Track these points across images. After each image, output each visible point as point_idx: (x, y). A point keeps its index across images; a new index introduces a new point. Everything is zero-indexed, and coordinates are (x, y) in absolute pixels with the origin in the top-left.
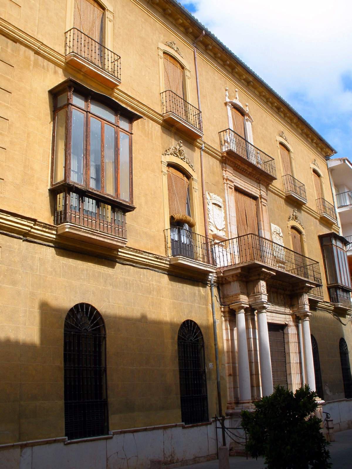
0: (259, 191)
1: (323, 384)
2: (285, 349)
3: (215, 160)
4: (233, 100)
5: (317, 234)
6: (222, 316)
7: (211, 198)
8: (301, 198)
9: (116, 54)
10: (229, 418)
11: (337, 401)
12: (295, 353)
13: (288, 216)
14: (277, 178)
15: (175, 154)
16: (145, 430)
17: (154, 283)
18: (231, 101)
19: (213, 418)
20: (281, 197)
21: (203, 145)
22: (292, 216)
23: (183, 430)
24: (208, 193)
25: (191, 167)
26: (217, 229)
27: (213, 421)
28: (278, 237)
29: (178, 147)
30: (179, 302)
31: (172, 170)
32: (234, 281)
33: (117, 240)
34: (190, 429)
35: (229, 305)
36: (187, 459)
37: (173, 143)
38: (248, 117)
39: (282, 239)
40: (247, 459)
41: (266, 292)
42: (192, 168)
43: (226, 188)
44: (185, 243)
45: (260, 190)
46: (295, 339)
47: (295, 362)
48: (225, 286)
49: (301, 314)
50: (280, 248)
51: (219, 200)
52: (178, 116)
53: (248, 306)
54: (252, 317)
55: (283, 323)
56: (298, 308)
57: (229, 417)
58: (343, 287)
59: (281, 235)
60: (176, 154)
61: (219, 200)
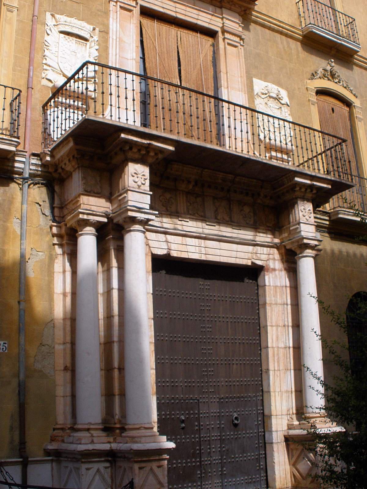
0: (220, 20)
2: (259, 318)
6: (54, 244)
7: (57, 22)
8: (340, 40)
10: (52, 461)
12: (284, 326)
13: (310, 69)
24: (53, 15)
28: (273, 104)
29: (329, 68)
37: (320, 64)
39: (285, 109)
41: (147, 187)
45: (222, 19)
46: (285, 297)
47: (282, 345)
49: (293, 243)
50: (276, 125)
51: (83, 27)
52: (318, 26)
53: (105, 220)
54: (119, 243)
56: (290, 232)
59: (285, 100)
61: (83, 27)
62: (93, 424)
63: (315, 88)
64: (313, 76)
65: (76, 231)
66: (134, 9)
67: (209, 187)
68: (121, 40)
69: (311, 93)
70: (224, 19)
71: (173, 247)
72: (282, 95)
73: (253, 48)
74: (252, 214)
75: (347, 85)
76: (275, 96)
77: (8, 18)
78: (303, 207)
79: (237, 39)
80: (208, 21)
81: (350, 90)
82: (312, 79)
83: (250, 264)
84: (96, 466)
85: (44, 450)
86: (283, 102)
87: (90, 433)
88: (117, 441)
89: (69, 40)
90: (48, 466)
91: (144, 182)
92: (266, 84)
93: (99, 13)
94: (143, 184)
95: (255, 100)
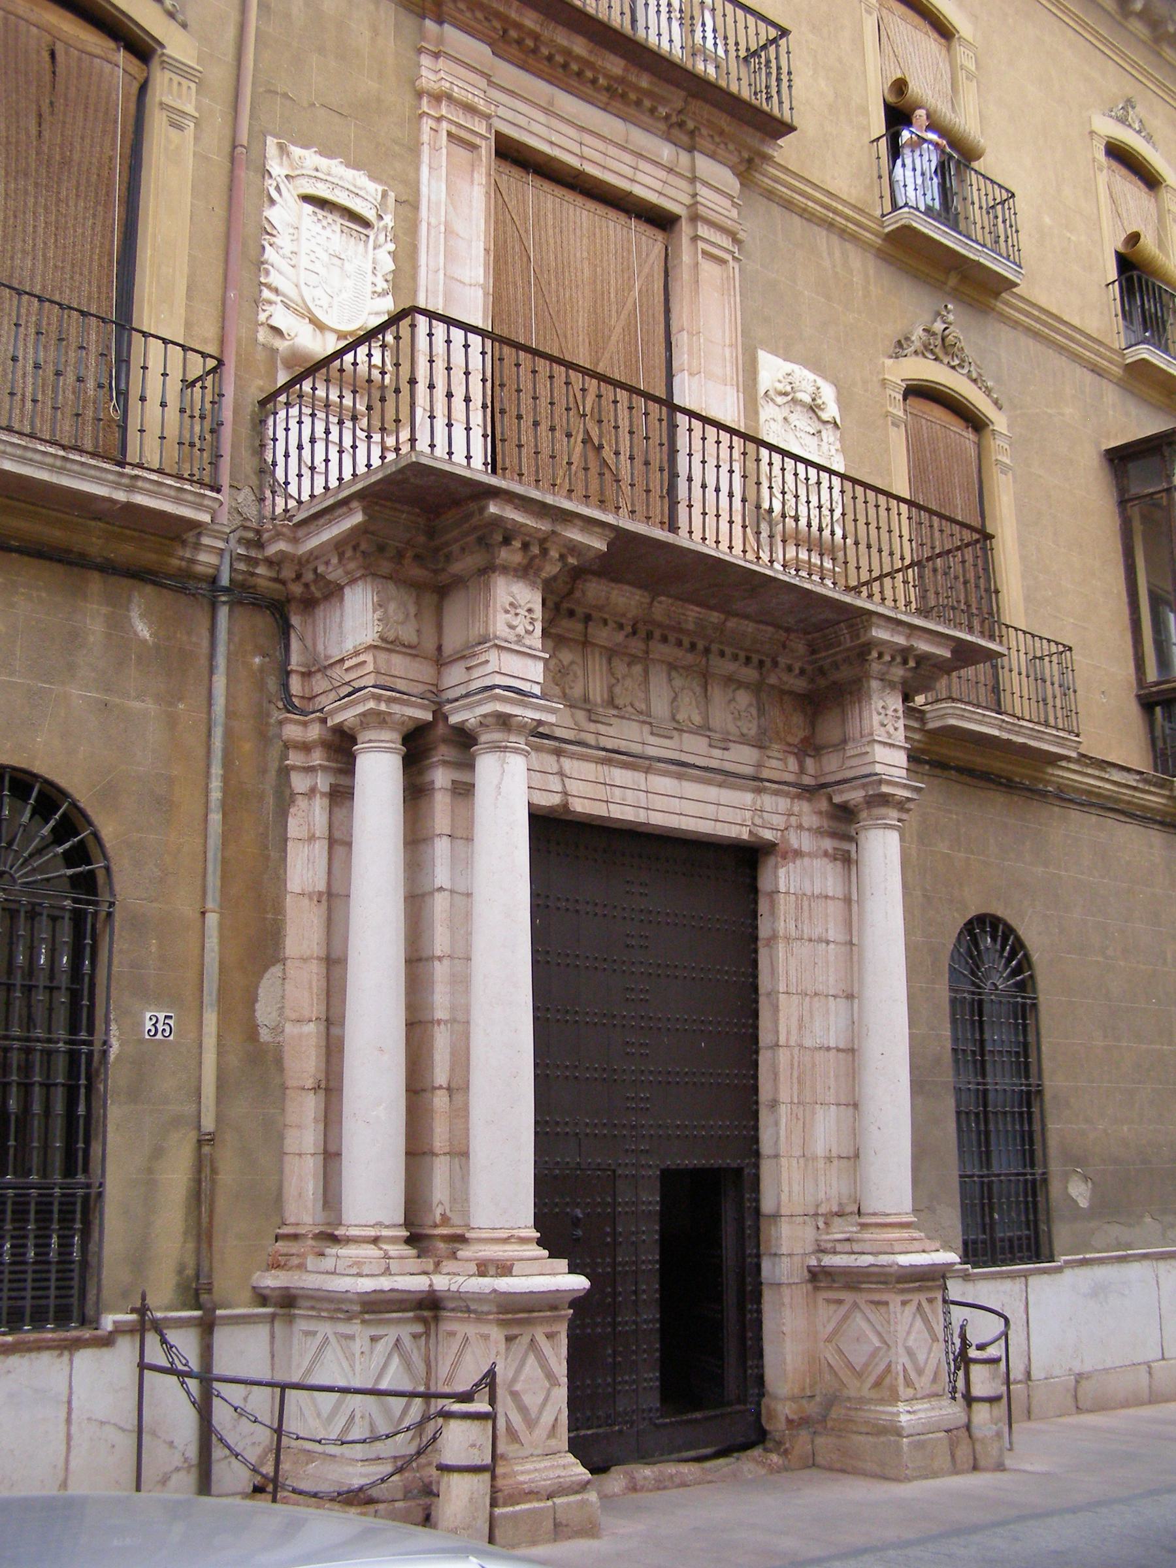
10: (273, 1317)
11: (1145, 1256)
13: (891, 330)
15: (926, 350)
19: (133, 1311)
20: (854, 238)
22: (918, 334)
24: (282, 148)
27: (119, 1330)
28: (801, 420)
31: (916, 403)
32: (353, 581)
33: (980, 718)
39: (829, 434)
41: (536, 640)
43: (425, 138)
48: (320, 612)
51: (360, 189)
59: (831, 411)
61: (360, 189)
62: (387, 1227)
64: (900, 347)
65: (354, 741)
66: (483, 143)
67: (664, 639)
68: (449, 231)
69: (894, 394)
70: (698, 185)
71: (573, 787)
72: (824, 399)
73: (762, 266)
74: (754, 711)
75: (980, 375)
76: (807, 399)
77: (172, 147)
78: (881, 704)
79: (726, 242)
80: (658, 185)
81: (987, 387)
82: (897, 358)
83: (745, 836)
84: (391, 1333)
85: (254, 1288)
86: (825, 416)
87: (381, 1249)
88: (445, 1271)
89: (325, 223)
90: (263, 1331)
91: (531, 628)
92: (789, 367)
93: (397, 148)
94: (527, 632)
95: (760, 410)
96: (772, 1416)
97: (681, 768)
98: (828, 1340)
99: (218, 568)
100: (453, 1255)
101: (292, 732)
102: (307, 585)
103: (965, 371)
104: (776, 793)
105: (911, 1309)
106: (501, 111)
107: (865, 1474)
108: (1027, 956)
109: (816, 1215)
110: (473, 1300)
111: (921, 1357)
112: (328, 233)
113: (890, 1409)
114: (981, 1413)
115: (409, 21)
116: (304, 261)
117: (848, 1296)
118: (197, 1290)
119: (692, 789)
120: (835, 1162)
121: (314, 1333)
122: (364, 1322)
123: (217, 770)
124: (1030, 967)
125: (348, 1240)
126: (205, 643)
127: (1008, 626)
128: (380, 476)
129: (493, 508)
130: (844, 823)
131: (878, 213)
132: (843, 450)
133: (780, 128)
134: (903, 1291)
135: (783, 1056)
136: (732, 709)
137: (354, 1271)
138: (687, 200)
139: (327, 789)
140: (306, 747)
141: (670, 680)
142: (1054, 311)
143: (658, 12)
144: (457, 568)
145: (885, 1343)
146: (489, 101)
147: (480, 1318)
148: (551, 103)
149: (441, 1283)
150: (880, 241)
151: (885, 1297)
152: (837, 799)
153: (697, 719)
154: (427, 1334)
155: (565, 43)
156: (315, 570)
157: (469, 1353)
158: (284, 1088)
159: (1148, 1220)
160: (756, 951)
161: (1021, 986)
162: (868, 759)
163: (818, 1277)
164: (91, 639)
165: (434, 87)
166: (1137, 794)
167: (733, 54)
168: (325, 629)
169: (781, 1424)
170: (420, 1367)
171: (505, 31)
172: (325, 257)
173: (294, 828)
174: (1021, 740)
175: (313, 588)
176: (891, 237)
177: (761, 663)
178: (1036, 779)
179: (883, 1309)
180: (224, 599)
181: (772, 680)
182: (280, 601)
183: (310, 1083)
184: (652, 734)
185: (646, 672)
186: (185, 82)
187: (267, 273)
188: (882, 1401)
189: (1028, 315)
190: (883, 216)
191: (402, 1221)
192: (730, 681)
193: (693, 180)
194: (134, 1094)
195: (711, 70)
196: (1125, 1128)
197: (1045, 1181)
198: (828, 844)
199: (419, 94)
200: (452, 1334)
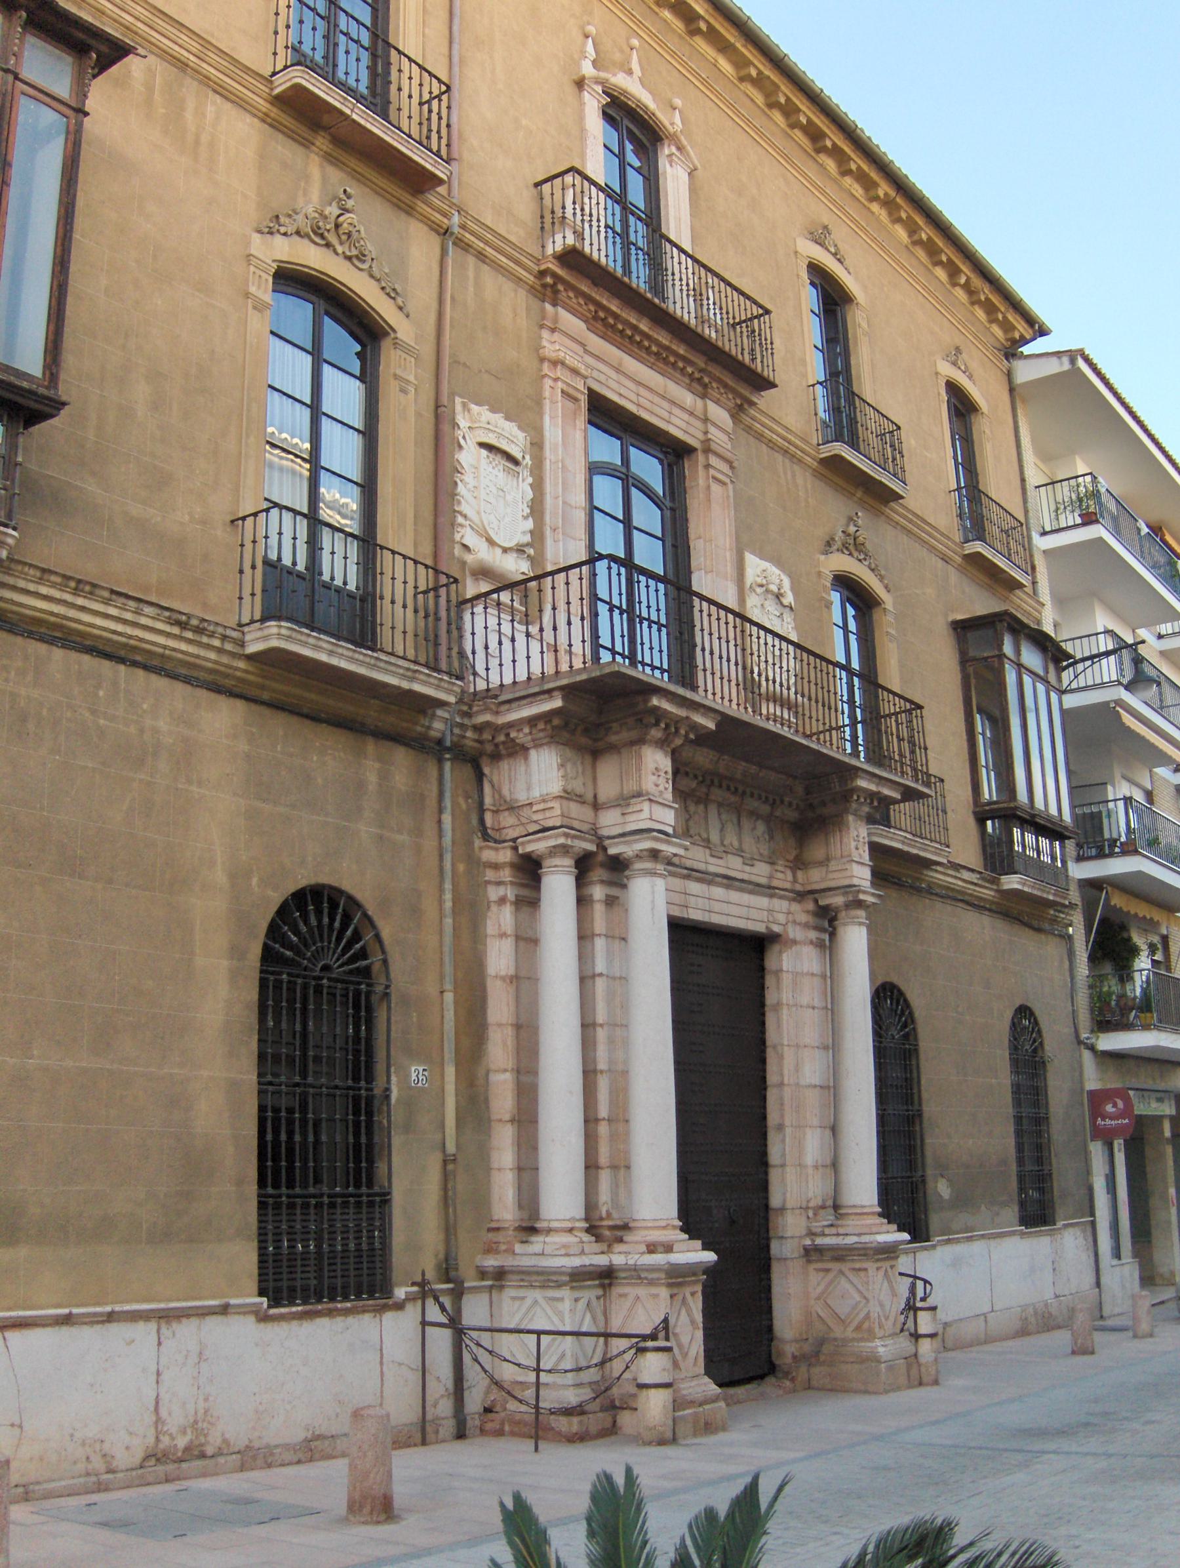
1: (929, 1172)
3: (508, 286)
4: (615, 75)
5: (946, 615)
9: (406, 56)
10: (491, 1287)
11: (983, 1236)
13: (821, 532)
14: (777, 382)
15: (317, 234)
16: (67, 1320)
17: (162, 725)
18: (603, 75)
19: (413, 1284)
21: (456, 219)
22: (839, 536)
23: (262, 1325)
24: (464, 405)
25: (392, 294)
26: (491, 542)
27: (410, 1298)
28: (771, 606)
30: (282, 809)
34: (295, 1323)
35: (514, 840)
36: (273, 1442)
38: (679, 149)
39: (788, 617)
40: (536, 1450)
41: (669, 795)
42: (394, 299)
43: (547, 394)
44: (338, 582)
51: (514, 439)
55: (760, 928)
57: (490, 1283)
58: (1034, 816)
59: (789, 599)
60: (322, 236)
61: (514, 439)
63: (274, 261)
76: (774, 588)
86: (785, 602)
96: (781, 1354)
97: (729, 881)
98: (818, 1298)
99: (444, 734)
100: (620, 1240)
101: (488, 855)
102: (497, 745)
103: (866, 563)
104: (781, 897)
105: (881, 1273)
106: (595, 374)
107: (856, 1392)
108: (911, 1014)
109: (808, 1208)
110: (643, 1270)
111: (887, 1308)
112: (495, 472)
113: (870, 1344)
114: (925, 1346)
115: (535, 303)
116: (483, 495)
117: (835, 1266)
118: (447, 1269)
119: (734, 896)
120: (821, 1169)
121: (523, 1298)
122: (572, 1288)
123: (448, 886)
124: (913, 1021)
125: (549, 1231)
126: (435, 789)
127: (382, 548)
128: (584, 677)
129: (655, 701)
130: (827, 920)
131: (815, 442)
132: (796, 628)
133: (763, 383)
134: (878, 1260)
135: (787, 1092)
136: (753, 837)
137: (563, 1252)
138: (701, 436)
139: (513, 899)
140: (496, 866)
141: (719, 814)
142: (919, 513)
143: (599, 232)
144: (613, 738)
145: (865, 1298)
146: (588, 366)
147: (652, 1283)
148: (620, 364)
149: (618, 1260)
150: (532, 278)
151: (864, 1265)
152: (821, 903)
153: (736, 844)
154: (604, 1295)
155: (634, 322)
156: (508, 735)
157: (640, 1309)
158: (489, 1120)
159: (983, 1208)
160: (763, 1014)
161: (906, 1037)
162: (848, 873)
163: (813, 1253)
164: (370, 787)
165: (553, 355)
166: (978, 889)
167: (725, 321)
168: (510, 776)
169: (788, 1360)
170: (601, 1318)
171: (596, 312)
172: (494, 491)
173: (491, 928)
174: (915, 851)
175: (501, 747)
176: (824, 462)
177: (774, 803)
178: (918, 879)
179: (862, 1274)
180: (447, 756)
181: (778, 813)
182: (476, 754)
183: (507, 1117)
184: (712, 856)
185: (706, 808)
186: (408, 357)
187: (459, 503)
188: (862, 1339)
189: (905, 517)
190: (274, 74)
191: (583, 1216)
192: (754, 815)
193: (706, 420)
194: (407, 1129)
195: (713, 335)
196: (971, 1142)
197: (924, 1181)
198: (813, 935)
199: (542, 360)
200: (624, 1296)
